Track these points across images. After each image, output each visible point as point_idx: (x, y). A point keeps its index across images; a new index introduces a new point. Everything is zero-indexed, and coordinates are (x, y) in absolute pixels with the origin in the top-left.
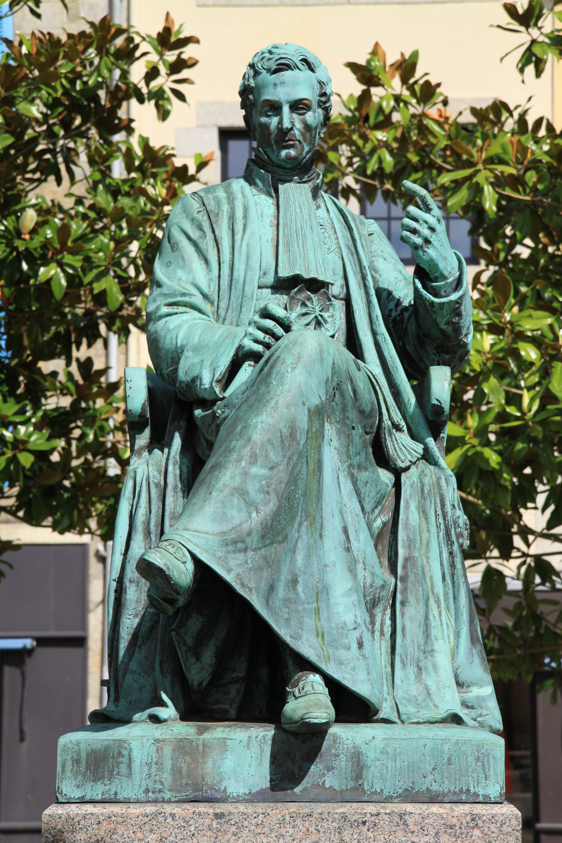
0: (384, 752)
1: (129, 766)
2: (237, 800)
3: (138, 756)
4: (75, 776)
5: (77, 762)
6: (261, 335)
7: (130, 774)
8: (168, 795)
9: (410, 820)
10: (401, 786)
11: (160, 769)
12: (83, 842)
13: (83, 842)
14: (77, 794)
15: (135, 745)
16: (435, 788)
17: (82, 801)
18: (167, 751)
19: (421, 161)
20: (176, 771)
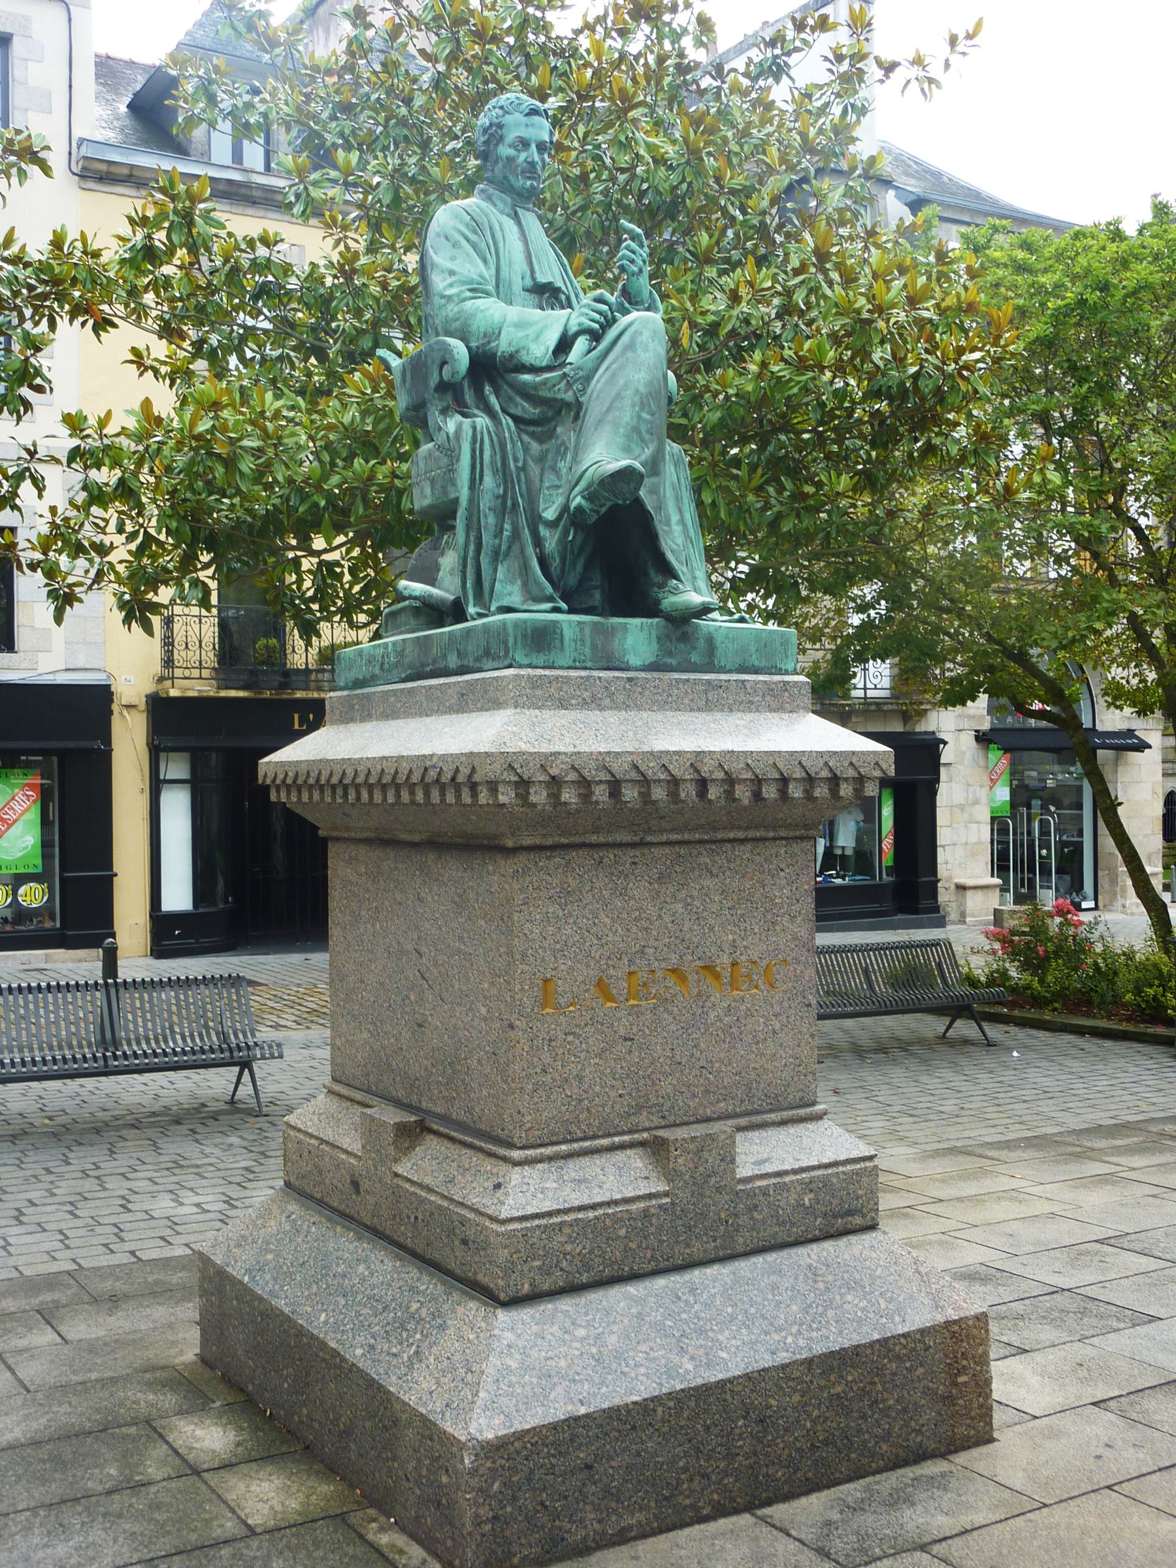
0: (727, 637)
1: (562, 641)
2: (636, 669)
3: (568, 634)
4: (524, 646)
5: (525, 636)
6: (596, 316)
7: (562, 648)
8: (589, 664)
9: (748, 685)
10: (738, 661)
11: (583, 645)
12: (4, 518)
13: (4, 518)
14: (526, 661)
15: (565, 626)
16: (756, 663)
17: (530, 666)
18: (587, 631)
19: (891, 399)
20: (594, 647)
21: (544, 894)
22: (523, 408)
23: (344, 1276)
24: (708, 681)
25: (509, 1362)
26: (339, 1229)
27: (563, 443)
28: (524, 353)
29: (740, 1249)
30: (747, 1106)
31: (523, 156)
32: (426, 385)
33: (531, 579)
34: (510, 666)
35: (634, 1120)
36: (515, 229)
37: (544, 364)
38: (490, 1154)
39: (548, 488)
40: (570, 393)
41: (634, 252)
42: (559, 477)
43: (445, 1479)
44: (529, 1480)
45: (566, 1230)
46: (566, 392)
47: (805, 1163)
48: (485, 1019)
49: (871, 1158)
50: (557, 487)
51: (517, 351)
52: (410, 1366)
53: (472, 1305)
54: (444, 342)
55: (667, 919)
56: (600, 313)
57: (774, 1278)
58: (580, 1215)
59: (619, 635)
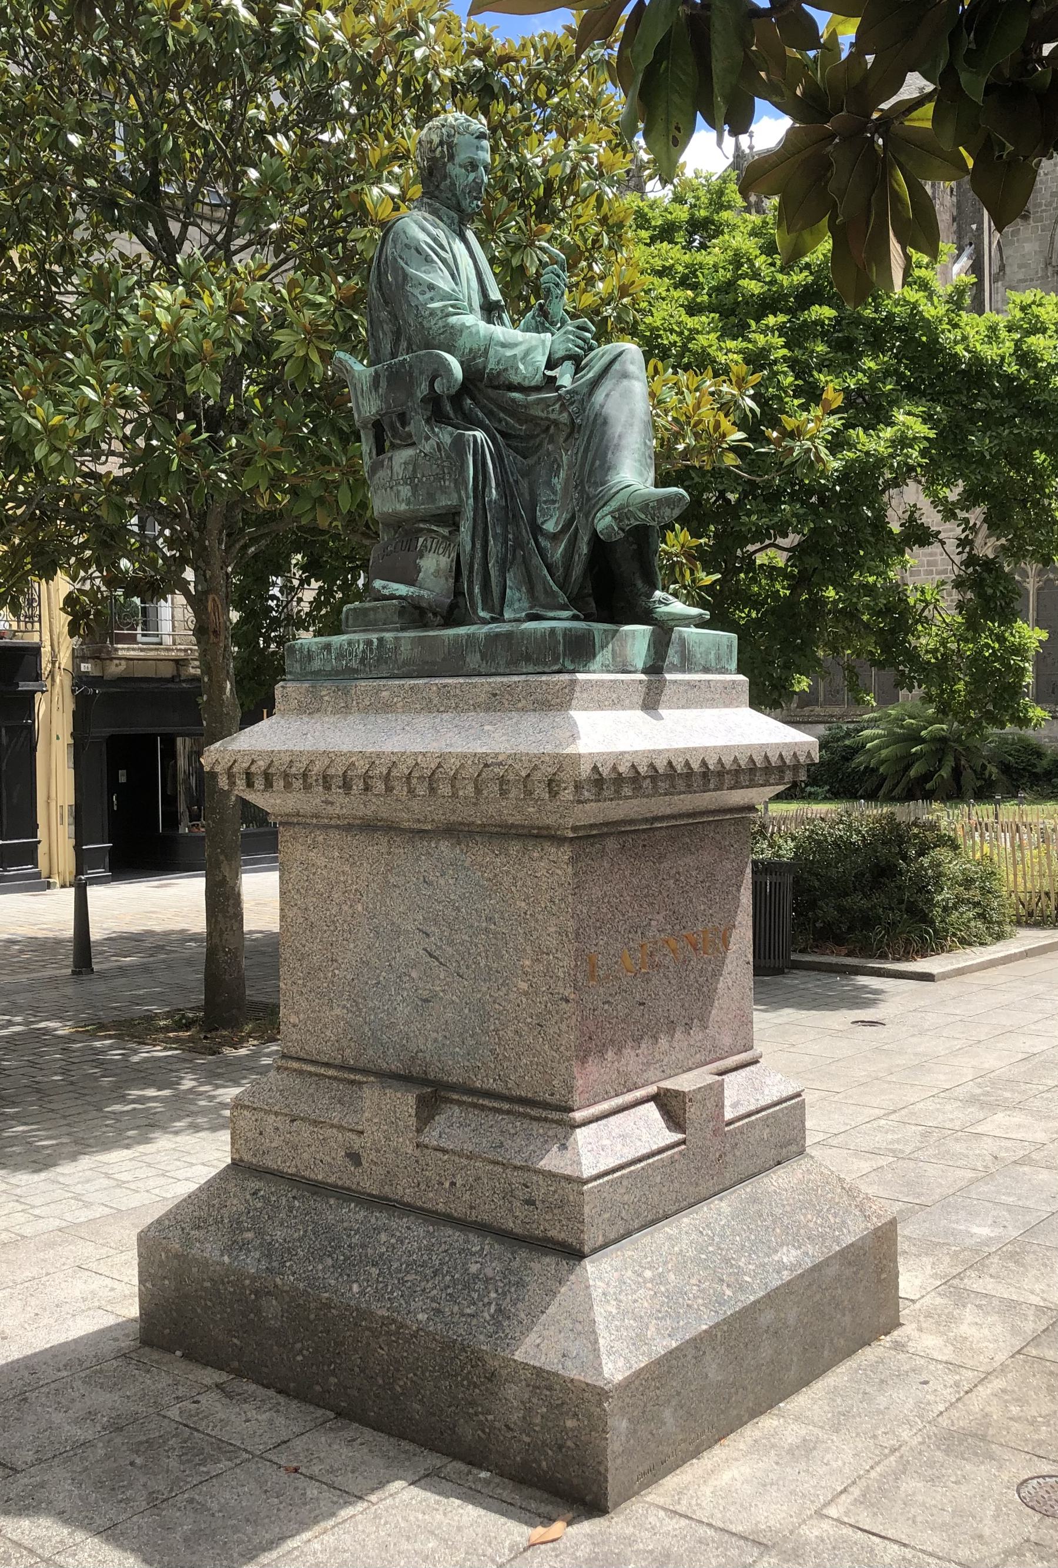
21: (589, 878)
22: (507, 423)
23: (364, 1246)
24: (688, 682)
25: (609, 1308)
26: (332, 1201)
27: (556, 460)
28: (511, 372)
29: (728, 1183)
30: (713, 1056)
31: (472, 176)
32: (411, 394)
33: (539, 587)
34: (559, 672)
35: (645, 1076)
36: (462, 246)
37: (533, 384)
38: (537, 1119)
39: (545, 502)
40: (565, 415)
41: (558, 276)
42: (555, 493)
43: (570, 1423)
44: (644, 1412)
45: (625, 1183)
46: (561, 412)
47: (763, 1103)
48: (526, 994)
49: (798, 1095)
50: (554, 502)
51: (506, 370)
52: (498, 1324)
53: (547, 1260)
54: (438, 355)
55: (665, 894)
56: (584, 340)
57: (757, 1207)
58: (632, 1168)
59: (630, 641)
